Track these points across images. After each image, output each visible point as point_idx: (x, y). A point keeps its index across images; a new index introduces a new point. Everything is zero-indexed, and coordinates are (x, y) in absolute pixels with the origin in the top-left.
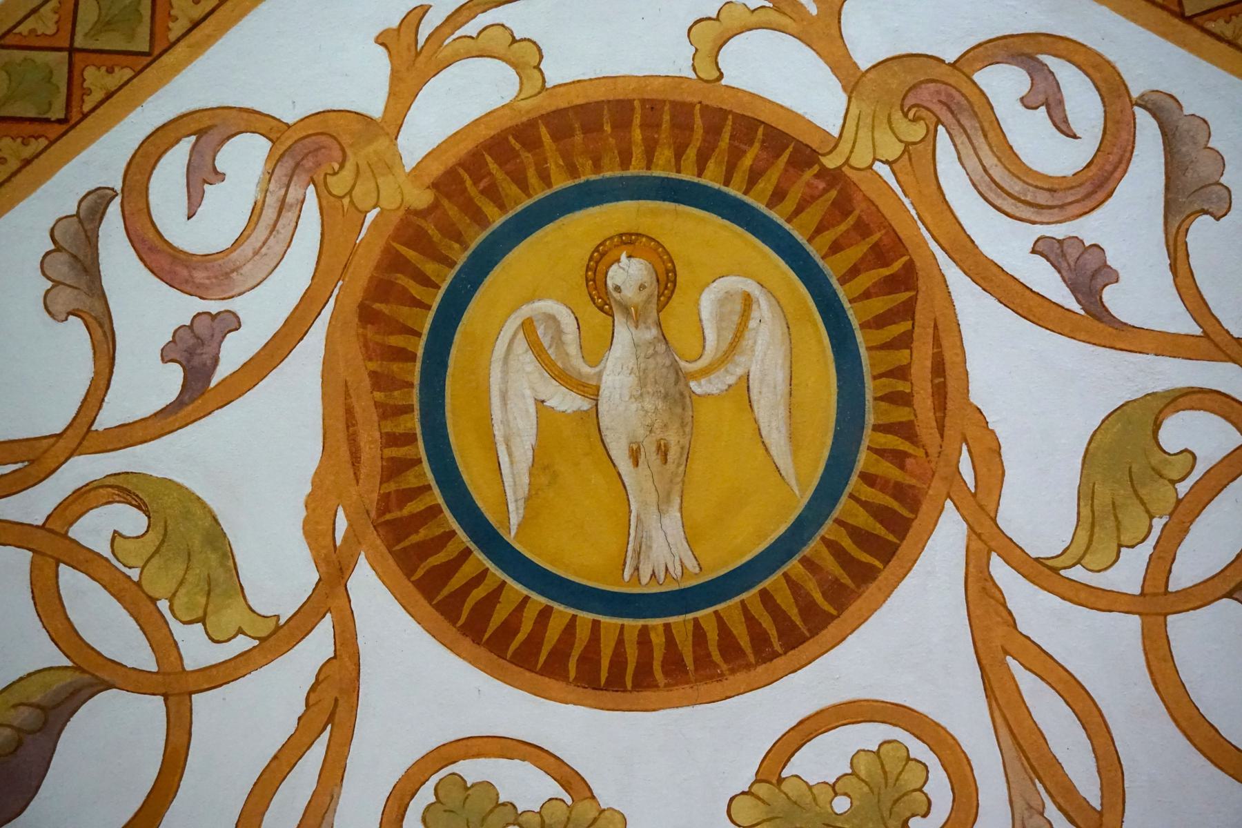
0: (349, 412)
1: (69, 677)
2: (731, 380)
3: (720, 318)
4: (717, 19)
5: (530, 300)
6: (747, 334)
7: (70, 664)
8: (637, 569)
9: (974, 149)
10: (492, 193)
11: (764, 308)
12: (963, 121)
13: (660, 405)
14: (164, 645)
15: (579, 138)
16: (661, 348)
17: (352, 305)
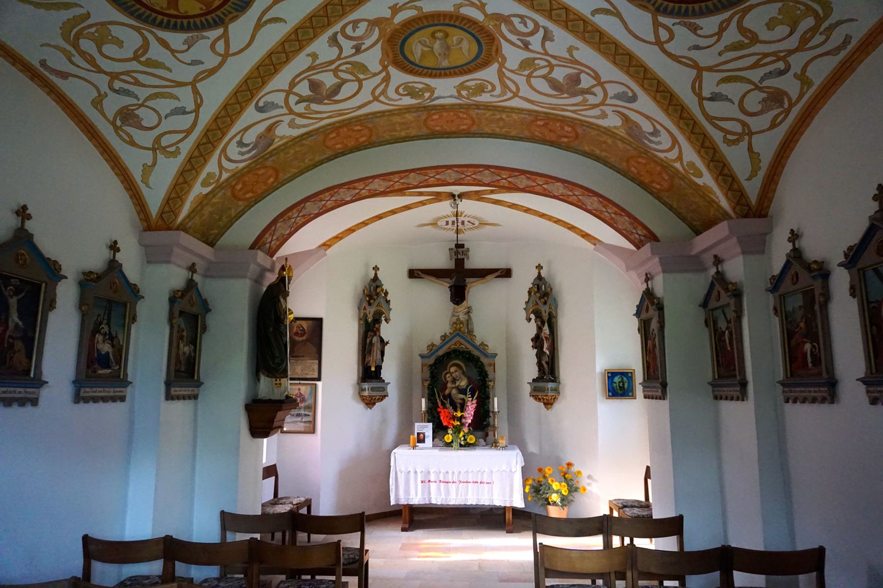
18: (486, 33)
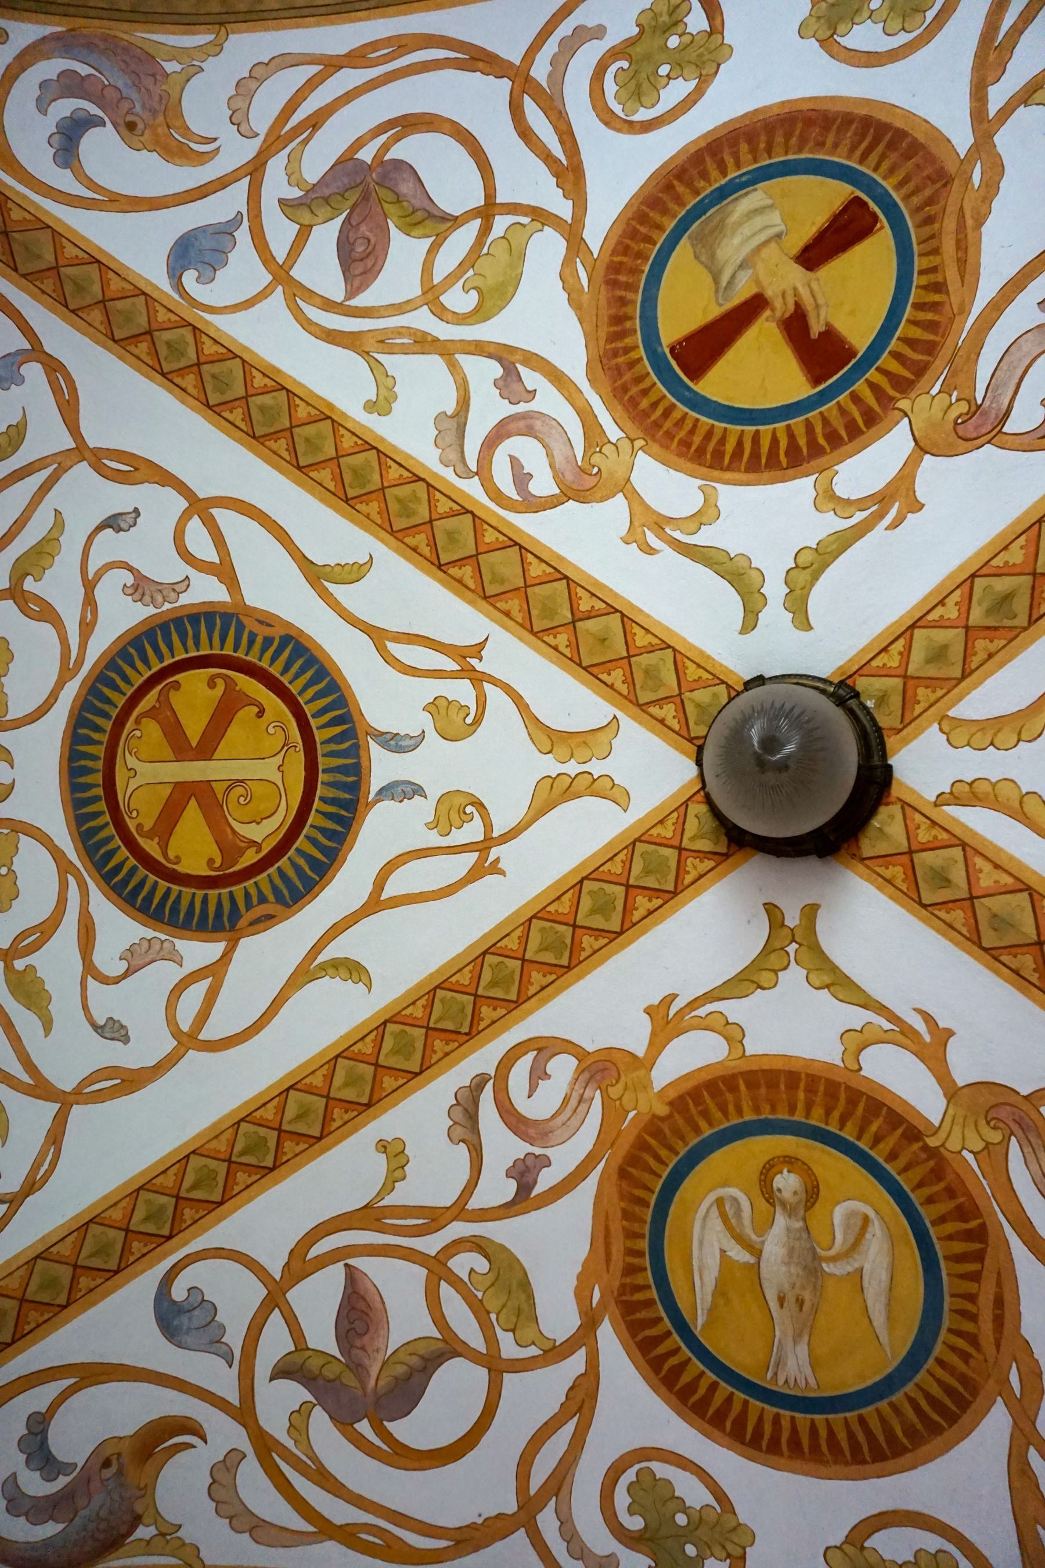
0: (607, 1228)
1: (441, 1345)
2: (850, 1269)
3: (847, 1227)
4: (861, 1031)
5: (725, 1185)
6: (863, 1242)
7: (440, 1337)
8: (776, 1374)
9: (1037, 1158)
10: (705, 1114)
11: (876, 1228)
12: (1030, 1138)
13: (801, 1273)
14: (491, 1340)
15: (763, 1091)
16: (805, 1235)
17: (618, 1160)
18: (950, 1193)
